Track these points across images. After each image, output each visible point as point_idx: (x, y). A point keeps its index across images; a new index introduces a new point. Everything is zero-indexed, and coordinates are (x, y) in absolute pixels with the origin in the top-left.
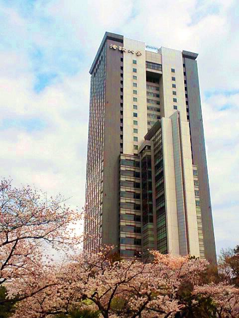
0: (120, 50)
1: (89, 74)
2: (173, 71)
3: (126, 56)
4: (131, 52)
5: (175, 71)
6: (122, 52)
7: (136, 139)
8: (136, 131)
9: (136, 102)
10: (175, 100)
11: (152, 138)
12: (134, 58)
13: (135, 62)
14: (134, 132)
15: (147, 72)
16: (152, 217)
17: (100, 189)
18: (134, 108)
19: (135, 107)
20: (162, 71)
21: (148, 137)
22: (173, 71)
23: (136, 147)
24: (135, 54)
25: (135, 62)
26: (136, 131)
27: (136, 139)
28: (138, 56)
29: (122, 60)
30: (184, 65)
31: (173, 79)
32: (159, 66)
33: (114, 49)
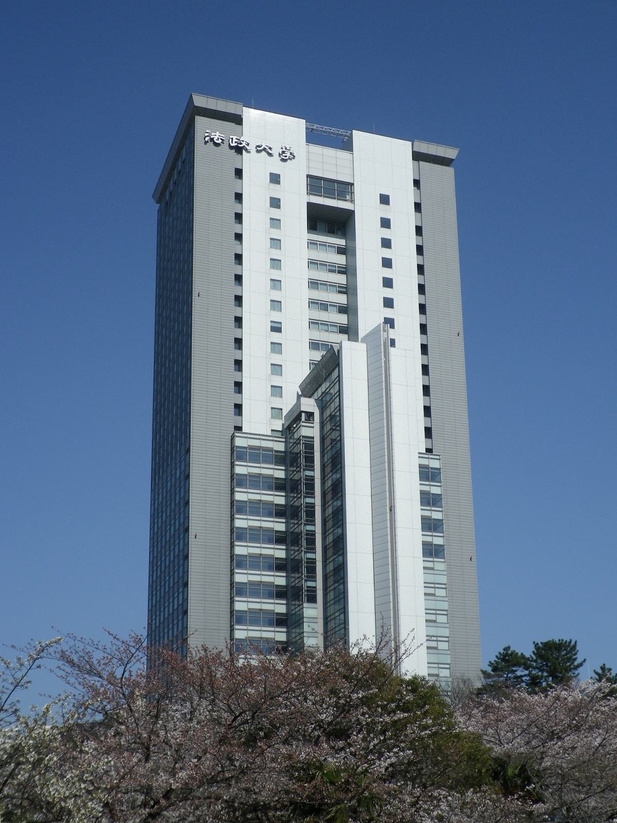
0: (234, 144)
1: (153, 202)
2: (385, 200)
3: (251, 163)
4: (264, 149)
5: (556, 636)
6: (239, 150)
7: (277, 390)
8: (277, 369)
9: (278, 314)
10: (388, 283)
11: (320, 385)
12: (275, 165)
13: (275, 179)
14: (272, 374)
15: (310, 206)
16: (313, 590)
17: (182, 495)
18: (272, 267)
19: (276, 305)
20: (352, 201)
21: (309, 388)
22: (385, 200)
23: (276, 412)
24: (276, 157)
25: (275, 179)
26: (277, 369)
27: (277, 390)
28: (283, 160)
29: (239, 173)
30: (417, 183)
31: (386, 223)
32: (344, 189)
33: (217, 145)
